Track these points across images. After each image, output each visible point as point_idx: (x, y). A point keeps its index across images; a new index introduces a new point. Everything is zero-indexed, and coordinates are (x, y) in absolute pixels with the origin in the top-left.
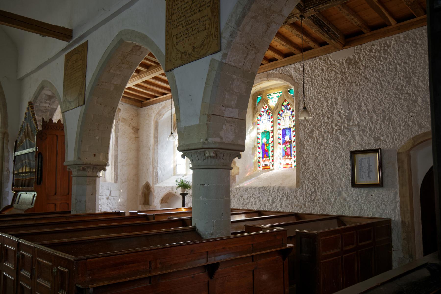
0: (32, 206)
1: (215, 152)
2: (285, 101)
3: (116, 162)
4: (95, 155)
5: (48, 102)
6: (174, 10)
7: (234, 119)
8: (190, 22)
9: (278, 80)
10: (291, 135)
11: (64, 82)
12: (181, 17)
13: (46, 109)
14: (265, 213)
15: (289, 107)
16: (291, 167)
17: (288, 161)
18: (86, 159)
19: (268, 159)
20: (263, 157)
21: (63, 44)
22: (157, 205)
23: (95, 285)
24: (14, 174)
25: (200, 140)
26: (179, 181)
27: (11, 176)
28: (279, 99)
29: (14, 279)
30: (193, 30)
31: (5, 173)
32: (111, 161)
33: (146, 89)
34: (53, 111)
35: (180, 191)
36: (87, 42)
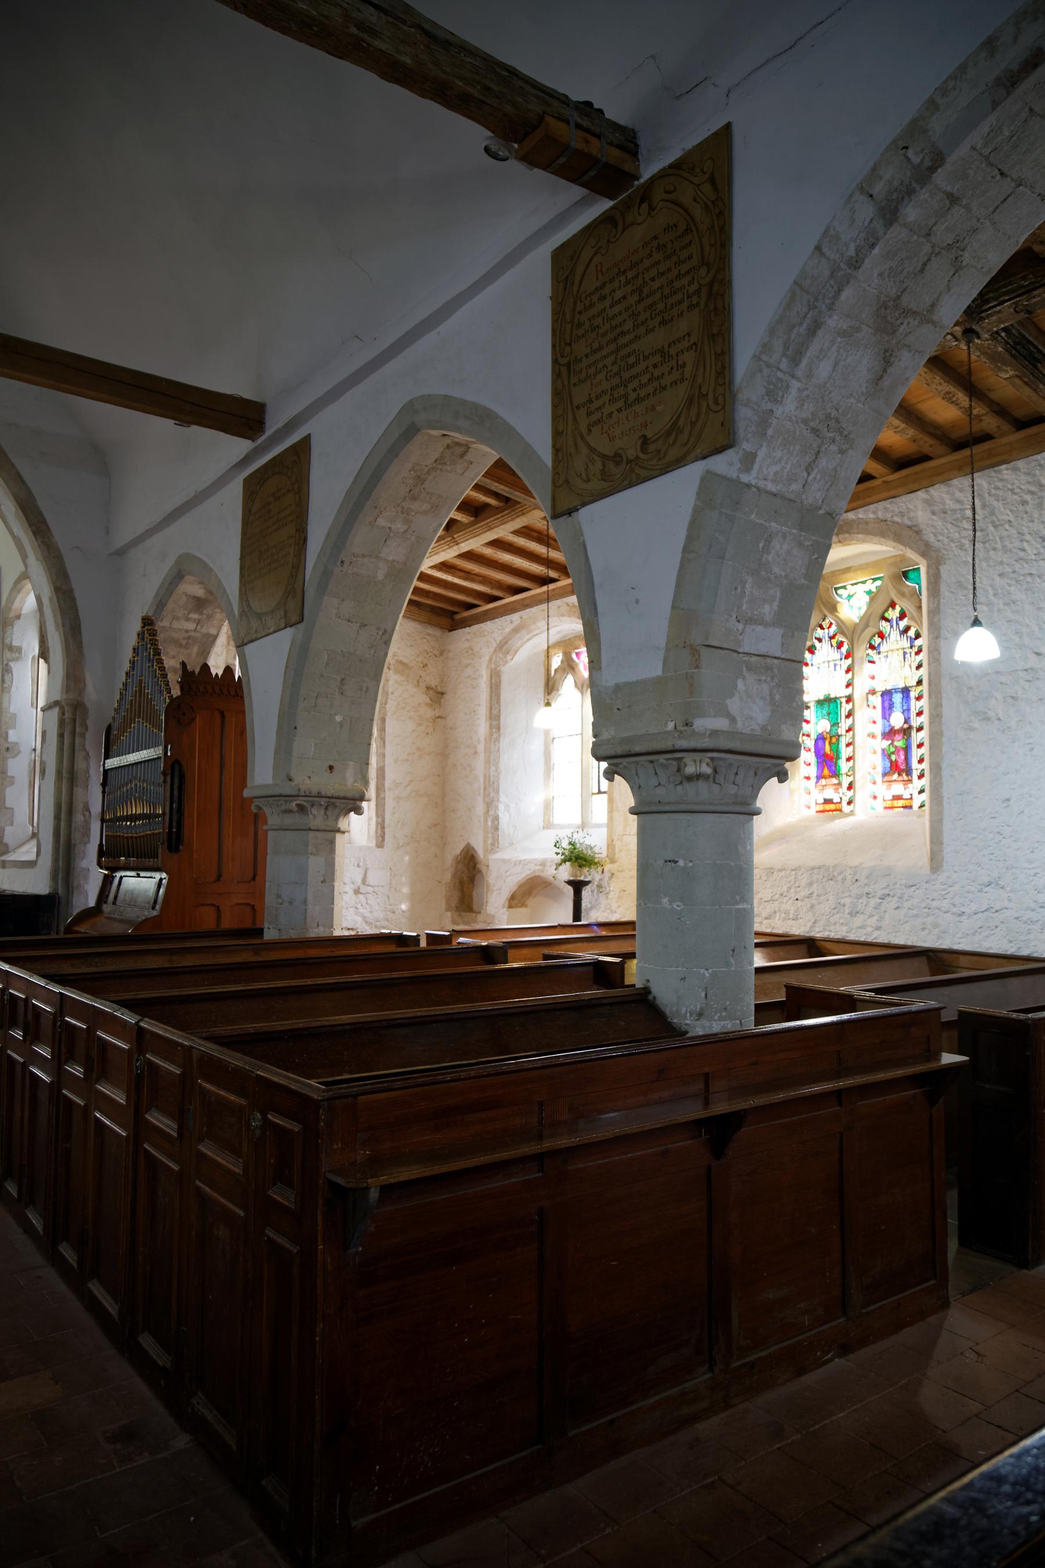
0: (155, 913)
1: (692, 760)
2: (893, 605)
3: (380, 789)
4: (331, 768)
6: (580, 325)
7: (769, 660)
8: (632, 360)
9: (870, 542)
10: (909, 710)
12: (601, 348)
13: (189, 638)
14: (828, 945)
15: (903, 624)
16: (911, 807)
17: (898, 789)
18: (307, 781)
19: (835, 781)
20: (819, 777)
21: (237, 447)
22: (499, 915)
23: (384, 1179)
24: (103, 820)
25: (666, 725)
26: (565, 844)
27: (96, 827)
28: (872, 600)
29: (128, 1135)
30: (641, 386)
31: (79, 818)
33: (468, 575)
35: (566, 872)
36: (306, 441)
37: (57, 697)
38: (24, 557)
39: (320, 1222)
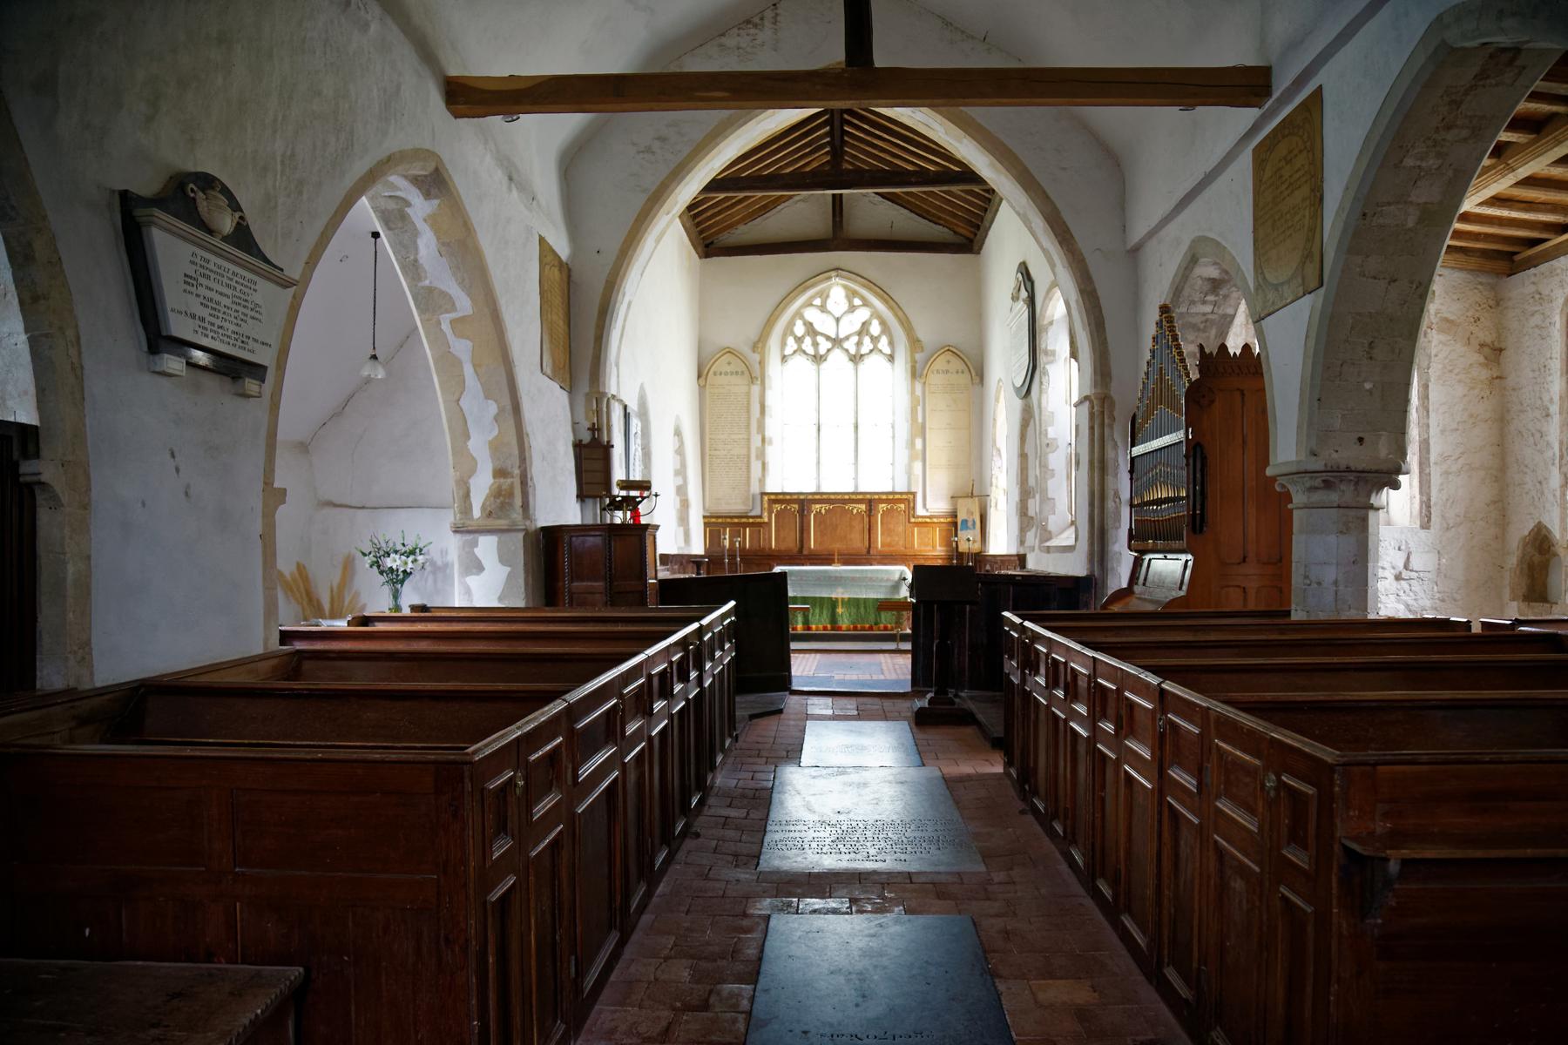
0: (1182, 593)
3: (1424, 463)
4: (1361, 440)
5: (1211, 298)
11: (1255, 231)
18: (1335, 455)
24: (1132, 506)
31: (1110, 504)
32: (1413, 459)
33: (1529, 205)
34: (1227, 322)
36: (1318, 93)
37: (1087, 392)
38: (1053, 266)
39: (1334, 885)
